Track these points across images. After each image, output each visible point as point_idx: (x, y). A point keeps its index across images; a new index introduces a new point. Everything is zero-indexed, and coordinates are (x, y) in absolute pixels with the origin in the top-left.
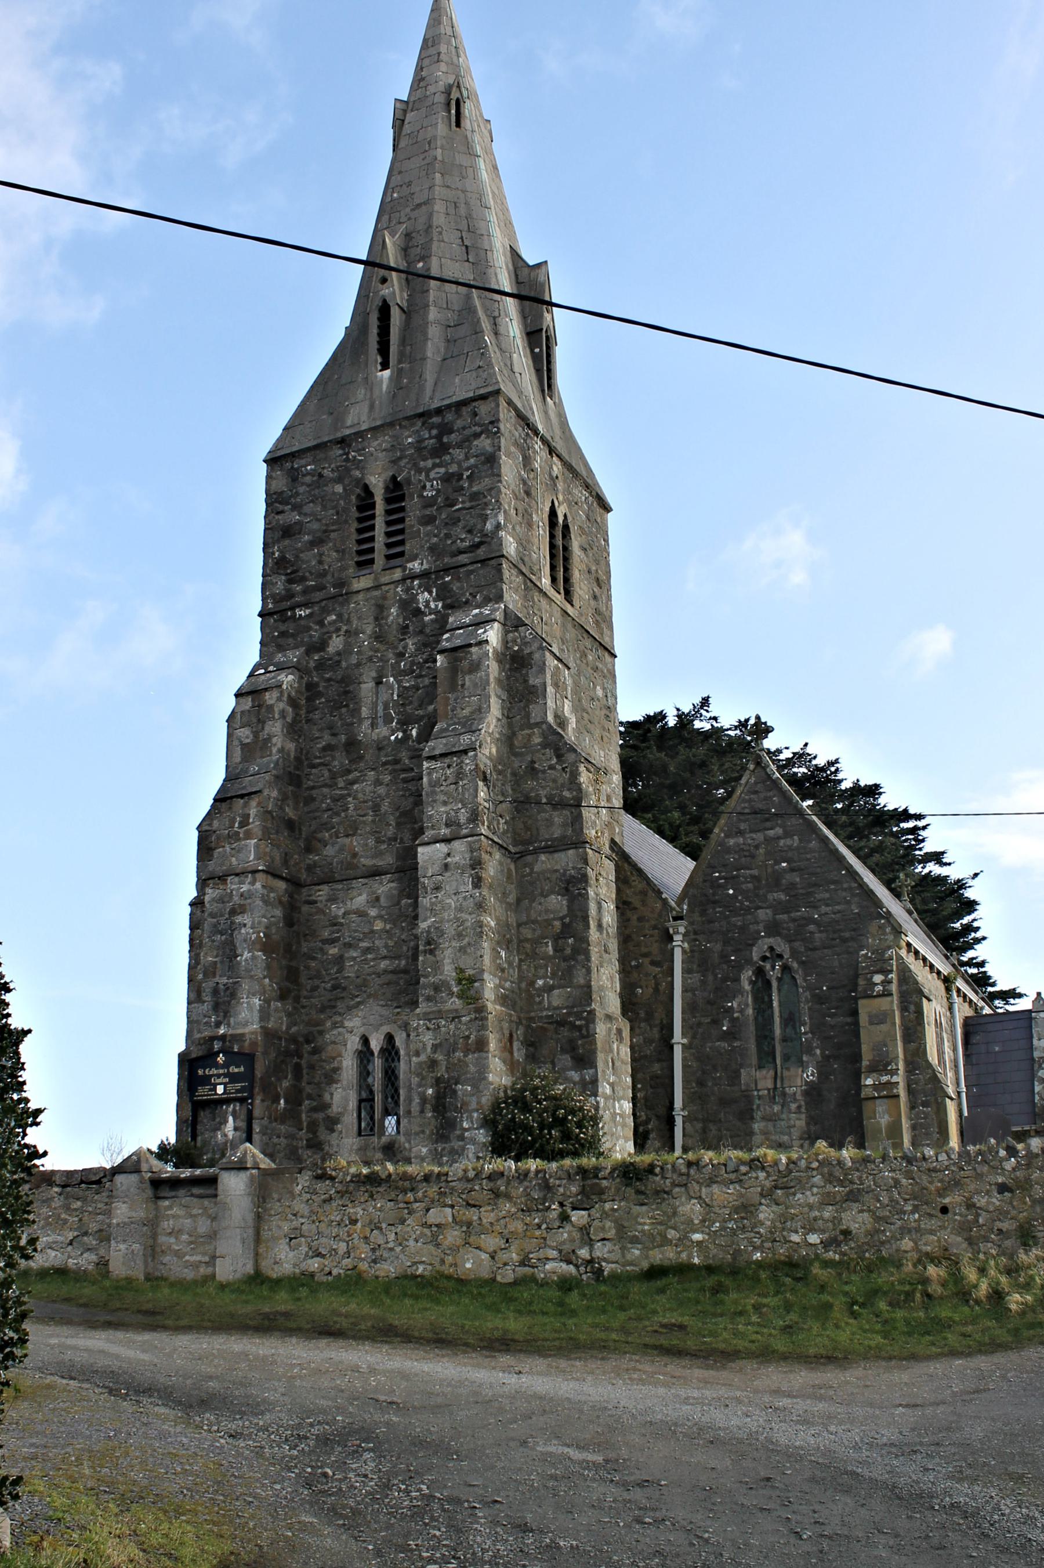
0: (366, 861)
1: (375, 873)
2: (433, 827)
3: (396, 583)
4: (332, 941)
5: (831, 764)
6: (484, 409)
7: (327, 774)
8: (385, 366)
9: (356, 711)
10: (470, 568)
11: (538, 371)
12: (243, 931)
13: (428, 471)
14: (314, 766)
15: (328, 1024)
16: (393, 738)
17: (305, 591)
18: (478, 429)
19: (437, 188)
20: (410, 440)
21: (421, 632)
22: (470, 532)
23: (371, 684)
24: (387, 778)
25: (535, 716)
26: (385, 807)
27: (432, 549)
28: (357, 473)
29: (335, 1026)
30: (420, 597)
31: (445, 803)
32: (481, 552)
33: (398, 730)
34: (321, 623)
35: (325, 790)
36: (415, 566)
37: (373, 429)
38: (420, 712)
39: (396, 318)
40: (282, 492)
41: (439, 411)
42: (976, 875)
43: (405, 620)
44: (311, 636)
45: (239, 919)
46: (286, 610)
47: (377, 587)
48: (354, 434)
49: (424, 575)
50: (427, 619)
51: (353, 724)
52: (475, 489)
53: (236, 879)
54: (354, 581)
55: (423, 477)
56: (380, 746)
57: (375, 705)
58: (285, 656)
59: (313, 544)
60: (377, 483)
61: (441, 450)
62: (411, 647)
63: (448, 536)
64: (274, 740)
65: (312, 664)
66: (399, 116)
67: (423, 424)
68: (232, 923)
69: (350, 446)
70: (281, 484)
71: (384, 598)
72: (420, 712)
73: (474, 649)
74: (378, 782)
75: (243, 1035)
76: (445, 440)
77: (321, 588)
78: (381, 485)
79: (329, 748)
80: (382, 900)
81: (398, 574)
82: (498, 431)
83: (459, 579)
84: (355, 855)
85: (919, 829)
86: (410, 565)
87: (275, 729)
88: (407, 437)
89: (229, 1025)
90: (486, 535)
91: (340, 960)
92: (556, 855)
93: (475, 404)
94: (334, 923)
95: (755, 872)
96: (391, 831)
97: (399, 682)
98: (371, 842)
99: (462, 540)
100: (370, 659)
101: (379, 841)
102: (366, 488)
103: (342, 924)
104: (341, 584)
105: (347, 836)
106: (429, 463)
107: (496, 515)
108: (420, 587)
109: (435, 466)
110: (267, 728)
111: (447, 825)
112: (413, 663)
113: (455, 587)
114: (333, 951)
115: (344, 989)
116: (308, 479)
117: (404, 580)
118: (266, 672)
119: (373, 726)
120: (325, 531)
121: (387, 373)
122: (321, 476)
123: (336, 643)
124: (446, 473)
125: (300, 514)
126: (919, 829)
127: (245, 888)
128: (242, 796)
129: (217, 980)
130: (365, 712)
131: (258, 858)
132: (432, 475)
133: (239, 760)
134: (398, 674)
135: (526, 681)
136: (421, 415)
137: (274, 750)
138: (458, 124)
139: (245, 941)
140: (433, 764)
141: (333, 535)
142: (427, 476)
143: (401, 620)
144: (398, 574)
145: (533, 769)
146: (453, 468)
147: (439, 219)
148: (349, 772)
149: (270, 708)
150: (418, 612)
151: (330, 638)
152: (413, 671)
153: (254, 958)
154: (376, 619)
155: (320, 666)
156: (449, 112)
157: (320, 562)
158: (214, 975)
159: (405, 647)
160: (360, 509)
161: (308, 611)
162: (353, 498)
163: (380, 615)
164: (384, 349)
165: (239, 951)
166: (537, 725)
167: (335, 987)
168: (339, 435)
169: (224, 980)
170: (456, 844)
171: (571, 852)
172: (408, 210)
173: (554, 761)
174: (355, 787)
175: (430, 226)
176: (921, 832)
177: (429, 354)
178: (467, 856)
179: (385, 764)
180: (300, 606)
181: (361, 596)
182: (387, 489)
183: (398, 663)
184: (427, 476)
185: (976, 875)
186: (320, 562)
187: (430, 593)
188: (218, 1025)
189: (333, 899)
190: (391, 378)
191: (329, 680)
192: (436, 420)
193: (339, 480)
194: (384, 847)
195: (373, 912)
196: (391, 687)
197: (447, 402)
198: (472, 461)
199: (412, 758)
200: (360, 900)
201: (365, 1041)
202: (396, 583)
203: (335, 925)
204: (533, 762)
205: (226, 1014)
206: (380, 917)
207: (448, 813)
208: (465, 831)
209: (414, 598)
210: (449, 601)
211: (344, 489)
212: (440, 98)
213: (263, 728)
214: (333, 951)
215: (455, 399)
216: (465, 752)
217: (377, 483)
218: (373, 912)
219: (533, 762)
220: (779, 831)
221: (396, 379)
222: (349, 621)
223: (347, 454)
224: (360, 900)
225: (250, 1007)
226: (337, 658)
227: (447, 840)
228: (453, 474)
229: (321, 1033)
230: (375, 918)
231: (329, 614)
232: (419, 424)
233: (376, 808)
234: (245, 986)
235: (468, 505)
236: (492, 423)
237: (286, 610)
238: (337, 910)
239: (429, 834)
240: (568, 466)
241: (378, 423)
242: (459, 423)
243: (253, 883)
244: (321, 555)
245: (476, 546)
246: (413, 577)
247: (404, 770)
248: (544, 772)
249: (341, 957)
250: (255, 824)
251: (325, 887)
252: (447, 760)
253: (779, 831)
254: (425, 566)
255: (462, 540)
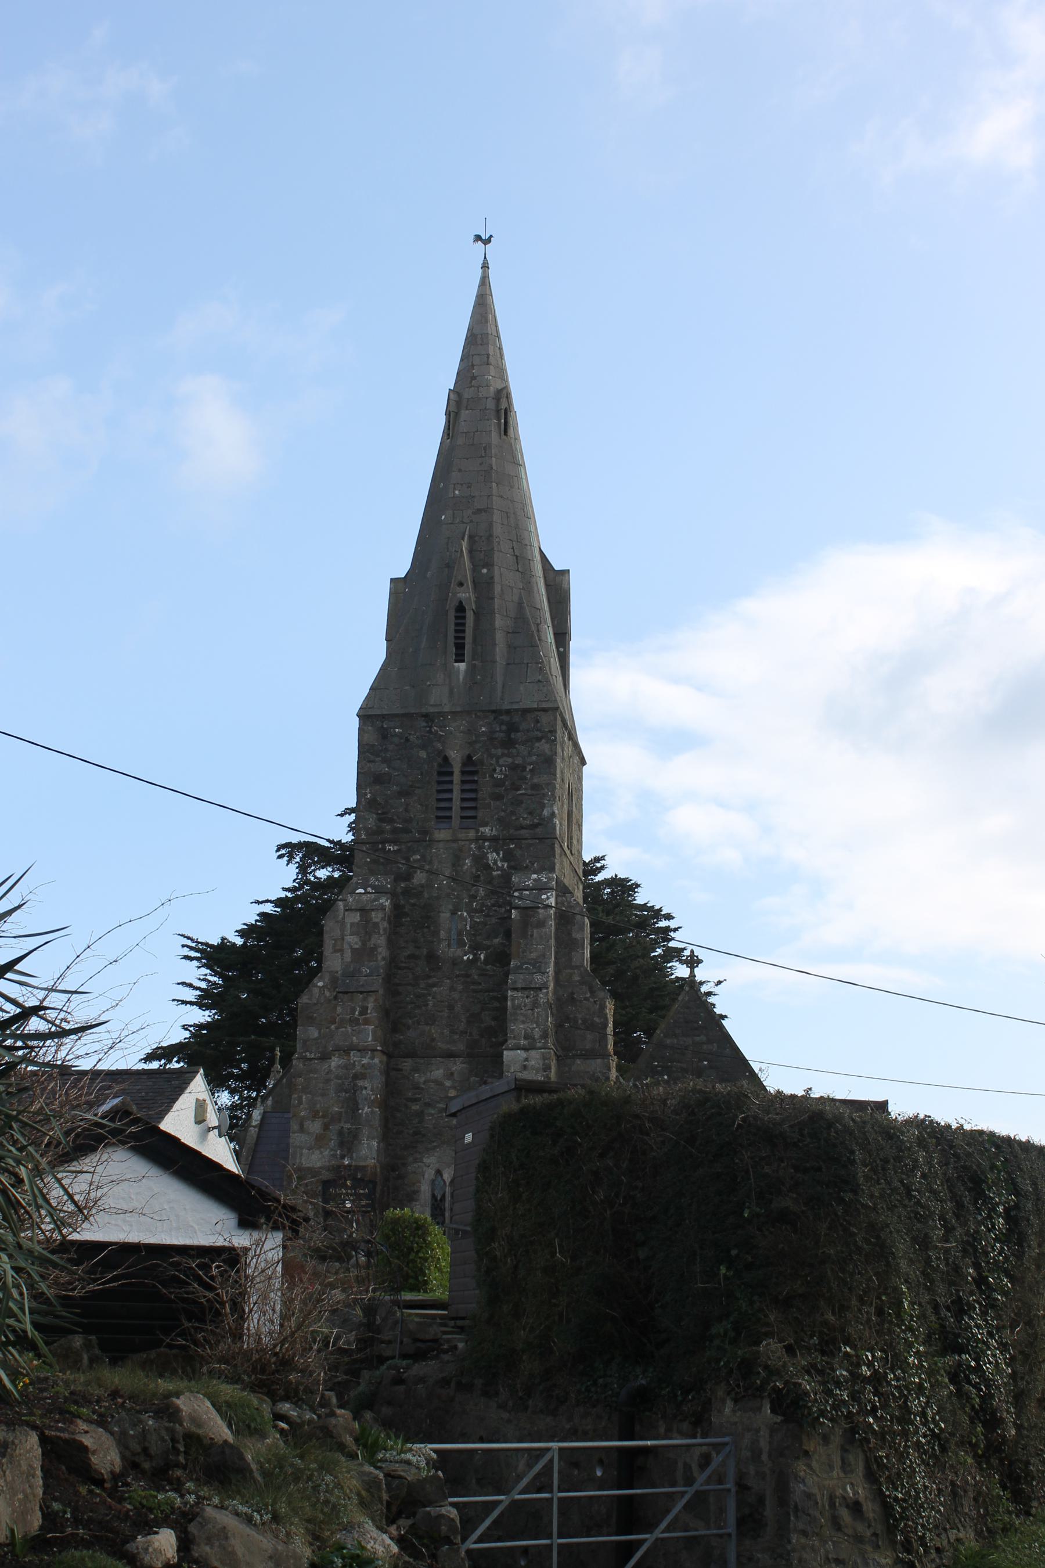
0: (444, 1046)
1: (450, 1055)
2: (514, 1038)
3: (471, 841)
4: (416, 1100)
5: (597, 859)
6: (545, 719)
7: (411, 976)
8: (460, 658)
9: (436, 933)
10: (530, 841)
11: (561, 667)
12: (364, 1092)
13: (498, 758)
14: (400, 968)
15: (410, 1159)
16: (465, 958)
17: (395, 831)
18: (540, 734)
19: (494, 498)
20: (483, 729)
21: (490, 883)
22: (530, 813)
23: (448, 915)
24: (460, 987)
25: (575, 961)
26: (458, 1008)
27: (500, 820)
28: (439, 746)
29: (415, 1160)
30: (489, 855)
31: (523, 1022)
32: (539, 830)
33: (469, 953)
34: (407, 859)
35: (409, 988)
36: (486, 830)
37: (454, 713)
38: (487, 942)
39: (470, 616)
40: (373, 746)
41: (508, 712)
42: (719, 982)
43: (477, 870)
44: (399, 868)
45: (360, 1083)
46: (378, 843)
47: (455, 841)
48: (438, 713)
49: (494, 839)
50: (495, 873)
51: (433, 942)
52: (535, 781)
53: (359, 1054)
54: (436, 832)
55: (493, 762)
56: (455, 962)
57: (450, 929)
58: (377, 880)
59: (401, 794)
60: (456, 756)
61: (509, 743)
62: (482, 892)
63: (513, 813)
64: (380, 950)
65: (399, 890)
66: (452, 409)
67: (495, 719)
68: (355, 1085)
69: (433, 721)
70: (372, 738)
71: (461, 850)
72: (487, 942)
73: (541, 911)
74: (452, 989)
75: (364, 1167)
76: (513, 736)
77: (406, 831)
78: (459, 760)
79: (411, 957)
80: (456, 1075)
81: (472, 834)
82: (555, 740)
83: (521, 848)
84: (433, 1040)
85: (671, 930)
86: (482, 829)
87: (380, 941)
88: (481, 726)
89: (352, 1158)
90: (543, 819)
91: (420, 1114)
92: (588, 1061)
93: (539, 713)
94: (416, 1087)
95: (684, 1066)
96: (462, 1026)
97: (471, 917)
98: (446, 1032)
99: (524, 819)
100: (448, 895)
101: (453, 1032)
102: (446, 759)
103: (423, 1089)
104: (425, 832)
105: (427, 1024)
106: (499, 752)
107: (552, 805)
108: (489, 848)
109: (503, 755)
110: (373, 941)
111: (525, 1038)
112: (483, 905)
113: (518, 853)
114: (415, 1107)
115: (424, 1135)
116: (396, 740)
117: (477, 839)
118: (366, 893)
119: (449, 946)
120: (411, 786)
121: (462, 666)
122: (407, 740)
123: (419, 878)
124: (513, 763)
125: (389, 767)
126: (671, 930)
127: (365, 1061)
128: (361, 993)
129: (342, 1124)
130: (443, 934)
131: (374, 1039)
132: (501, 761)
133: (349, 960)
134: (471, 912)
135: (569, 934)
136: (493, 711)
137: (380, 958)
138: (506, 433)
139: (366, 1099)
140: (515, 994)
141: (417, 791)
142: (497, 762)
143: (474, 870)
144: (472, 834)
145: (573, 998)
146: (518, 761)
147: (498, 530)
148: (429, 977)
149: (376, 925)
150: (487, 867)
151: (416, 872)
152: (483, 911)
153: (372, 1112)
154: (454, 865)
155: (406, 892)
156: (499, 419)
157: (406, 810)
158: (340, 1121)
159: (477, 891)
160: (440, 774)
161: (396, 848)
162: (435, 764)
163: (457, 861)
164: (460, 647)
165: (361, 1106)
166: (577, 967)
167: (416, 1134)
168: (424, 710)
169: (348, 1126)
170: (533, 1053)
171: (599, 1061)
172: (470, 512)
173: (588, 995)
174: (434, 989)
175: (491, 536)
176: (672, 934)
177: (498, 659)
178: (541, 1063)
179: (458, 976)
180: (390, 842)
181: (441, 845)
182: (464, 765)
183: (471, 902)
184: (497, 762)
185: (719, 982)
186: (406, 810)
187: (498, 854)
188: (343, 1157)
189: (416, 1070)
190: (466, 671)
191: (413, 905)
192: (504, 718)
193: (423, 747)
194: (456, 1037)
195: (448, 1083)
196: (465, 920)
197: (515, 707)
198: (534, 758)
199: (479, 975)
200: (438, 1073)
201: (439, 1172)
202: (471, 841)
203: (418, 1088)
204: (573, 993)
205: (350, 1151)
206: (454, 1087)
207: (526, 1030)
208: (539, 1045)
209: (484, 856)
210: (513, 863)
211: (428, 754)
212: (491, 404)
213: (370, 939)
214: (415, 1107)
215: (522, 706)
216: (540, 989)
217: (456, 756)
218: (448, 1083)
219: (573, 993)
220: (703, 1038)
221: (472, 670)
222: (430, 863)
223: (431, 727)
224: (438, 1073)
225: (370, 1147)
226: (420, 889)
227: (525, 1049)
228: (518, 766)
229: (404, 1165)
230: (450, 1088)
231: (414, 854)
232: (492, 717)
233: (451, 1007)
234: (365, 1131)
235: (529, 792)
236: (550, 731)
237: (378, 843)
238: (419, 1078)
239: (511, 1042)
240: (570, 733)
241: (459, 709)
242: (523, 726)
243: (372, 1058)
244: (408, 805)
245: (536, 826)
246: (485, 839)
247: (474, 983)
248: (581, 1001)
249: (422, 1112)
250: (372, 1014)
251: (410, 1060)
252: (526, 992)
253: (703, 1038)
254: (494, 833)
255: (524, 819)
